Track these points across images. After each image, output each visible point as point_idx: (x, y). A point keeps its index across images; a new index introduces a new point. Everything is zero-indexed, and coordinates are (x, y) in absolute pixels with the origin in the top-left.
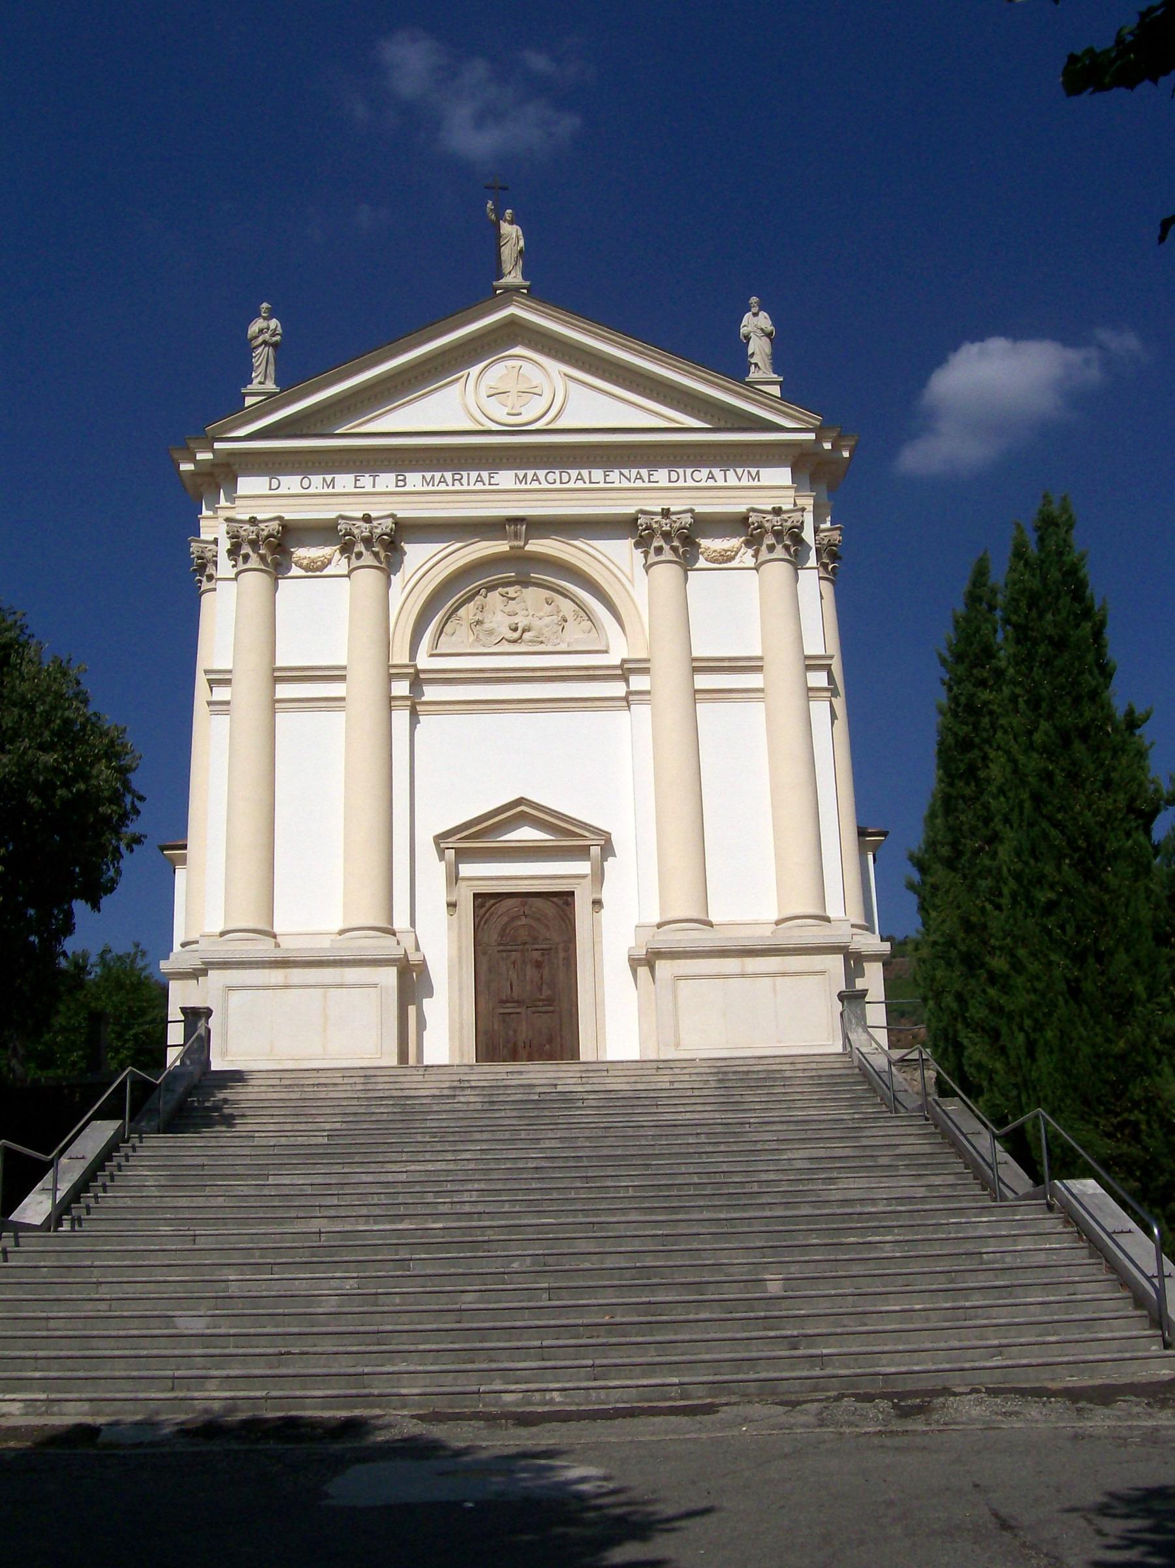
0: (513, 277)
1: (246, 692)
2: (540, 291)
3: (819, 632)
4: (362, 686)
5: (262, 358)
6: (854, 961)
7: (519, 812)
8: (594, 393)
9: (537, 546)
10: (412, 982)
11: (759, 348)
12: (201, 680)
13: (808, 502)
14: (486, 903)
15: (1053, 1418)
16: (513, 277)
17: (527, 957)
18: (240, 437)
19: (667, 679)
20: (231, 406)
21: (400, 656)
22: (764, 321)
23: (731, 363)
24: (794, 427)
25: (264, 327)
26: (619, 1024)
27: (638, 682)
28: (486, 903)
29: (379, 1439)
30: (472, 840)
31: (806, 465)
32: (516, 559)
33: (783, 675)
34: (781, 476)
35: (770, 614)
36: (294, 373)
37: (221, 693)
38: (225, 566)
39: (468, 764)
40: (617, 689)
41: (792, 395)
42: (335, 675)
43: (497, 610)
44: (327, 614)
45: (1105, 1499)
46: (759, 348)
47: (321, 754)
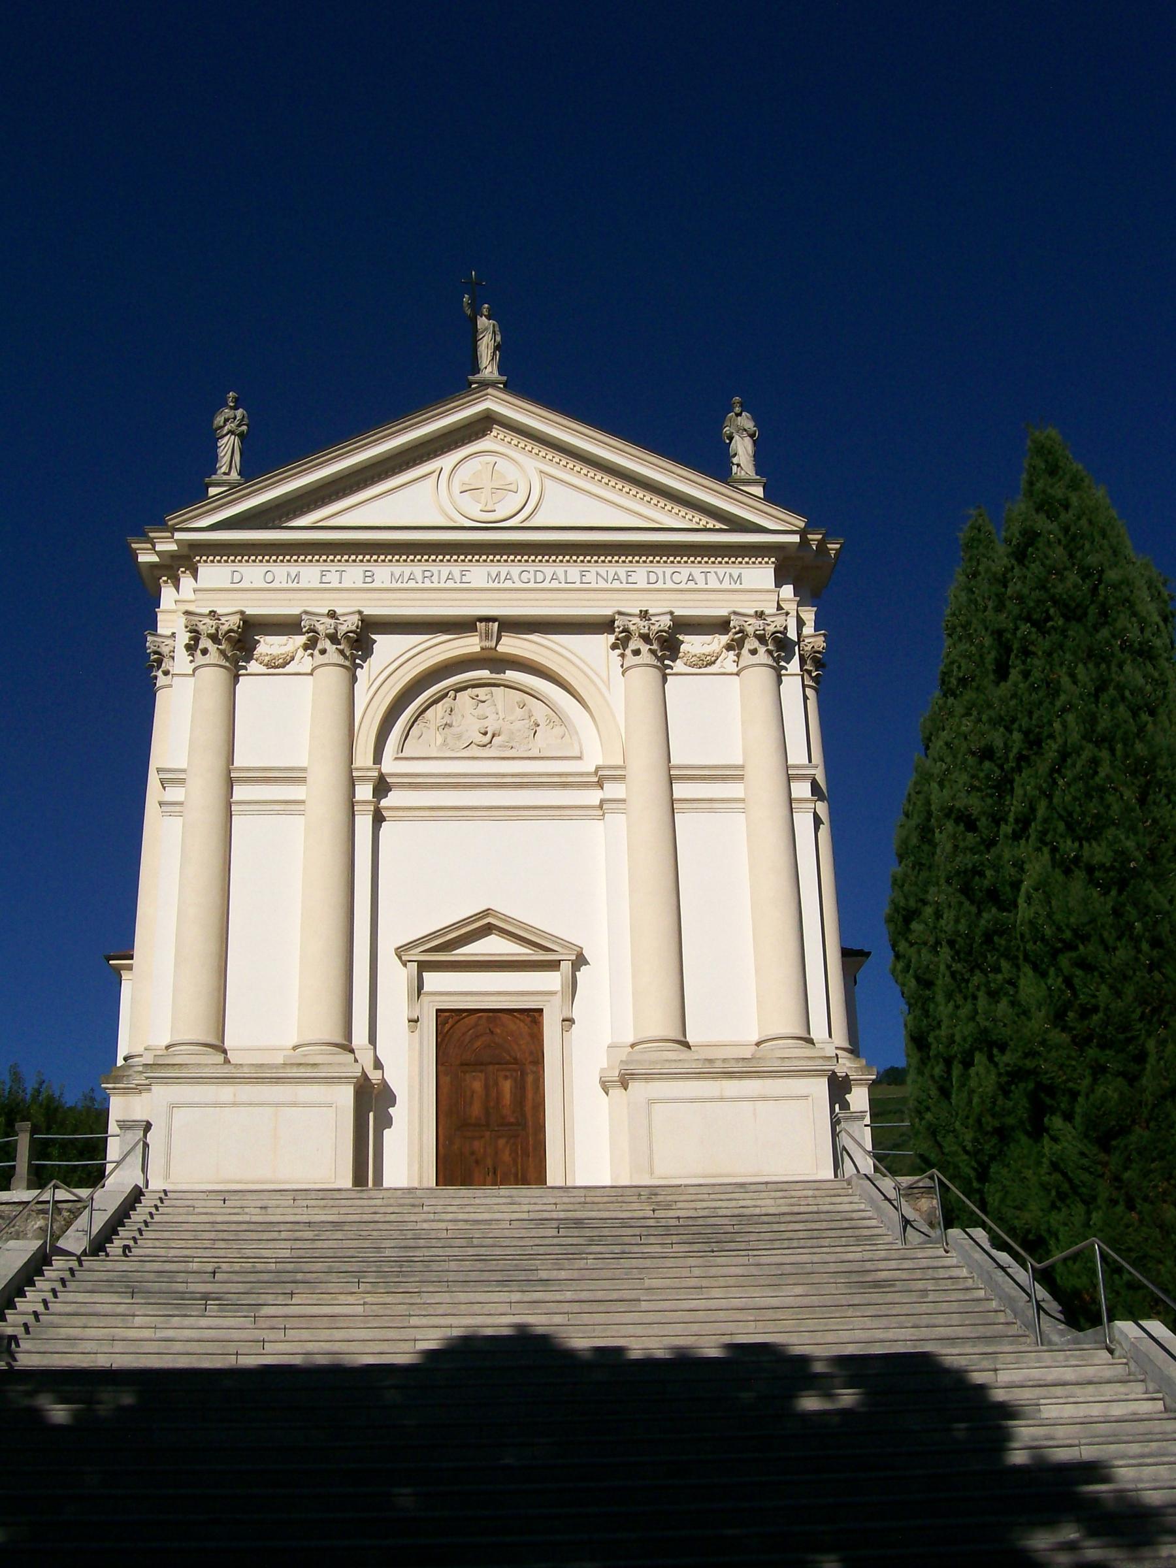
0: (489, 369)
2: (518, 382)
4: (321, 793)
5: (228, 448)
6: (839, 1088)
7: (484, 925)
9: (511, 645)
10: (372, 1101)
11: (743, 450)
12: (153, 780)
13: (809, 615)
14: (451, 1022)
16: (489, 369)
17: (491, 1086)
18: (200, 525)
19: (641, 788)
20: (192, 492)
22: (746, 421)
23: (716, 465)
24: (781, 526)
26: (591, 1140)
27: (613, 790)
28: (451, 1022)
30: (440, 952)
31: (790, 566)
32: (489, 653)
33: (763, 785)
34: (762, 575)
35: (749, 723)
36: (258, 464)
37: (174, 794)
38: (181, 662)
39: (431, 875)
40: (593, 797)
41: (771, 497)
42: (294, 777)
43: (472, 712)
44: (290, 711)
46: (743, 450)
47: (285, 859)
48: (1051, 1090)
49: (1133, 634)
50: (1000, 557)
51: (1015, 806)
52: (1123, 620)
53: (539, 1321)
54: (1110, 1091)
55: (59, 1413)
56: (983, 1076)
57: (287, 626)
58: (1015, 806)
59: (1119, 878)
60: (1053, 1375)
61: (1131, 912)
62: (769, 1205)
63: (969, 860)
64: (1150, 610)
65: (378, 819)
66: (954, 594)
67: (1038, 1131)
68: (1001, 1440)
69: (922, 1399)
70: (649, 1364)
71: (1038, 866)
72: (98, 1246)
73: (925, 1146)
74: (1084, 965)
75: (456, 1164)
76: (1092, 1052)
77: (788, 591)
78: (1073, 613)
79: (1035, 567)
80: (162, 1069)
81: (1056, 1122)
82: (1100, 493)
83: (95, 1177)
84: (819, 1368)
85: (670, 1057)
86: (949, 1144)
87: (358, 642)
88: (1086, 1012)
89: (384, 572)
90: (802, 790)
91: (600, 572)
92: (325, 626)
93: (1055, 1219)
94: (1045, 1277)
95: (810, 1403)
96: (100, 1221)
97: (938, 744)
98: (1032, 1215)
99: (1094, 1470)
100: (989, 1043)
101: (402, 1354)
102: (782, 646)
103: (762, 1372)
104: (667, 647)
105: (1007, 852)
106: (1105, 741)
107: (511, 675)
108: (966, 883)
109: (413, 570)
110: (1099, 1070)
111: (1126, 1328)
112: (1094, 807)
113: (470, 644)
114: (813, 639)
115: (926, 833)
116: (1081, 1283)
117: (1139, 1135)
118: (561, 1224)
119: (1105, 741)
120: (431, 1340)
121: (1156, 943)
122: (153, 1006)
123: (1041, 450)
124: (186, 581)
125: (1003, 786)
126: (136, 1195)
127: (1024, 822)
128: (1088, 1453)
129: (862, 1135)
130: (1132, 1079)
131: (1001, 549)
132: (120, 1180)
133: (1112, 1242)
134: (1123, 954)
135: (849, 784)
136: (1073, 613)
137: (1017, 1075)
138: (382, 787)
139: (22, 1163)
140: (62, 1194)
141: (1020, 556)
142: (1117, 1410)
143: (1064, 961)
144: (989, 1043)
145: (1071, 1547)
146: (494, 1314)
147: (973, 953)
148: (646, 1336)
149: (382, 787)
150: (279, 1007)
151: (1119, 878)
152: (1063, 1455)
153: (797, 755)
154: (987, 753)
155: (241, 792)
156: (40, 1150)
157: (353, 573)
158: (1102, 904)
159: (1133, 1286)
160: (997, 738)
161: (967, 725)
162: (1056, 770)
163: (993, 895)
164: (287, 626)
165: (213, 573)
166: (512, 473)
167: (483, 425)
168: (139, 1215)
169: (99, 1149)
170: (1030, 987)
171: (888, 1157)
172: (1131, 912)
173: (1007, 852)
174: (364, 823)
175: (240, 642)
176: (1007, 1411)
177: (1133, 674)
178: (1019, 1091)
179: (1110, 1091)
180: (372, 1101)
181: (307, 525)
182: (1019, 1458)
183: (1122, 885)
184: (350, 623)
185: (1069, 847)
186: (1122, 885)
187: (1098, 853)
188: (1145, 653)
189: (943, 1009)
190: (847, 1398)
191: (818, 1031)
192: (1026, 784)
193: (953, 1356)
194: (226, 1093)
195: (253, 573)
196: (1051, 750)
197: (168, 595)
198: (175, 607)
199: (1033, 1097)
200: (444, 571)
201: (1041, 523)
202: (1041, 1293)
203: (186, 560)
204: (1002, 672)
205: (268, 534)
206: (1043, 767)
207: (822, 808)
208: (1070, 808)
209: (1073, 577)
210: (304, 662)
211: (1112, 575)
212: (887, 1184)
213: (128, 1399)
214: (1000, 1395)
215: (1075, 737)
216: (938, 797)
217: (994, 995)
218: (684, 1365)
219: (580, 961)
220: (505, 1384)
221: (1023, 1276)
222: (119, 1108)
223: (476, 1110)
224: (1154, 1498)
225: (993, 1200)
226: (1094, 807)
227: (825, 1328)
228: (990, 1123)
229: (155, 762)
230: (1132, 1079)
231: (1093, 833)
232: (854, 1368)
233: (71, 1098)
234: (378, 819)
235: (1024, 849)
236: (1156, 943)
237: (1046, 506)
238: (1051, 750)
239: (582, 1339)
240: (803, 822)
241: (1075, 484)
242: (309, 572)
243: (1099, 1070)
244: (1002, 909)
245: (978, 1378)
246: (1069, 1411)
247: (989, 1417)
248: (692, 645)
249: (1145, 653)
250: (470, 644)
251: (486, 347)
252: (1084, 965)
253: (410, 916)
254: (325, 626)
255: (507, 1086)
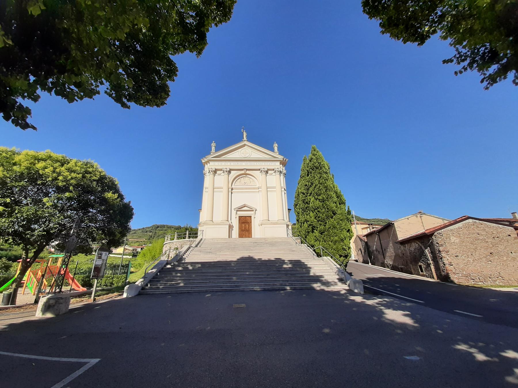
0: (245, 138)
1: (210, 190)
2: (249, 140)
3: (283, 184)
4: (225, 190)
5: (213, 148)
7: (245, 206)
10: (231, 227)
11: (276, 149)
13: (284, 168)
15: (19, 215)
16: (245, 138)
17: (245, 225)
18: (210, 157)
19: (264, 189)
20: (208, 153)
21: (230, 186)
22: (276, 145)
23: (272, 150)
24: (281, 157)
25: (213, 145)
27: (260, 189)
30: (239, 209)
31: (283, 163)
32: (245, 173)
33: (278, 189)
34: (278, 163)
35: (277, 182)
36: (217, 149)
37: (207, 190)
38: (208, 174)
40: (258, 190)
41: (280, 154)
42: (221, 188)
43: (243, 180)
44: (221, 180)
45: (132, 104)
46: (276, 149)
47: (221, 198)
48: (314, 227)
49: (325, 170)
50: (308, 161)
52: (323, 169)
53: (251, 255)
54: (322, 227)
56: (306, 225)
57: (221, 170)
58: (310, 192)
59: (323, 201)
60: (316, 263)
61: (325, 205)
62: (279, 240)
65: (232, 193)
66: (302, 166)
67: (313, 232)
68: (309, 272)
70: (265, 261)
71: (313, 199)
72: (196, 246)
73: (298, 233)
74: (318, 211)
75: (241, 236)
76: (320, 222)
78: (317, 168)
79: (312, 162)
80: (205, 223)
81: (315, 231)
82: (320, 153)
83: (196, 237)
84: (286, 261)
85: (268, 221)
87: (229, 172)
88: (319, 217)
89: (232, 163)
90: (283, 189)
92: (225, 170)
93: (315, 243)
94: (314, 250)
95: (285, 266)
96: (197, 243)
97: (300, 184)
98: (312, 242)
100: (307, 221)
103: (279, 262)
104: (267, 172)
106: (321, 184)
108: (303, 201)
109: (236, 163)
110: (321, 225)
111: (325, 257)
112: (320, 192)
113: (243, 172)
114: (285, 172)
115: (298, 195)
116: (319, 251)
119: (321, 184)
121: (328, 209)
122: (204, 216)
123: (313, 148)
125: (308, 189)
126: (202, 239)
128: (321, 274)
129: (290, 232)
130: (325, 226)
132: (199, 238)
133: (323, 247)
134: (323, 210)
135: (288, 189)
136: (317, 168)
137: (310, 225)
138: (232, 189)
140: (192, 239)
141: (310, 161)
142: (324, 268)
143: (316, 211)
144: (307, 221)
145: (319, 287)
146: (246, 254)
147: (305, 210)
148: (265, 257)
149: (232, 189)
150: (220, 215)
151: (323, 201)
153: (282, 185)
154: (306, 185)
155: (215, 190)
156: (190, 234)
157: (228, 163)
158: (321, 204)
159: (326, 252)
160: (307, 183)
162: (315, 187)
163: (307, 203)
164: (221, 170)
165: (211, 163)
166: (247, 151)
167: (244, 145)
169: (197, 234)
170: (312, 214)
172: (325, 205)
174: (230, 193)
175: (215, 171)
176: (310, 268)
177: (325, 175)
178: (310, 227)
179: (322, 227)
180: (231, 227)
181: (223, 158)
182: (311, 274)
183: (323, 202)
184: (229, 169)
185: (316, 197)
186: (323, 202)
187: (320, 198)
188: (326, 173)
189: (301, 217)
190: (290, 266)
191: (285, 219)
192: (311, 189)
193: (303, 261)
194: (213, 226)
195: (216, 163)
196: (314, 185)
197: (206, 166)
198: (207, 168)
199: (312, 228)
200: (240, 163)
201: (313, 157)
202: (314, 252)
204: (308, 175)
205: (218, 158)
207: (286, 192)
210: (223, 174)
211: (322, 163)
212: (294, 238)
213: (200, 266)
214: (309, 266)
216: (300, 191)
217: (307, 215)
218: (269, 261)
219: (256, 210)
220: (248, 263)
222: (200, 228)
223: (243, 228)
224: (330, 280)
225: (307, 241)
226: (320, 192)
227: (287, 256)
229: (205, 186)
230: (325, 226)
231: (320, 195)
232: (291, 262)
233: (194, 227)
234: (232, 193)
235: (311, 197)
236: (328, 209)
237: (314, 155)
238: (314, 185)
239: (257, 257)
240: (283, 193)
241: (317, 152)
242: (223, 163)
243: (321, 225)
244: (76, 75)
245: (306, 263)
247: (307, 269)
248: (270, 172)
249: (326, 173)
250: (243, 172)
251: (245, 134)
252: (318, 211)
253: (236, 204)
254: (225, 170)
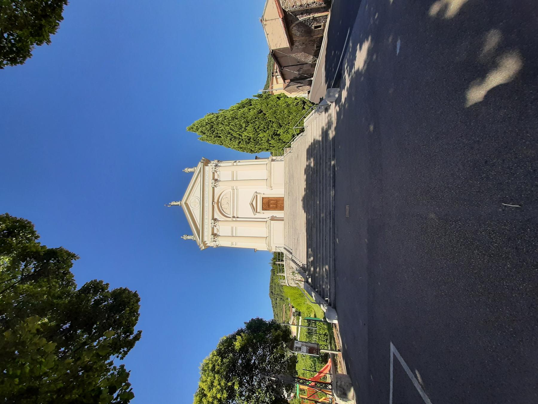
0: (178, 203)
1: (234, 240)
2: (180, 199)
3: (230, 163)
4: (234, 224)
5: (189, 237)
6: (273, 160)
8: (250, 223)
9: (216, 200)
10: (273, 219)
11: (190, 170)
12: (232, 246)
13: (212, 162)
14: (263, 209)
16: (178, 203)
17: (272, 204)
18: (199, 241)
19: (234, 184)
20: (195, 241)
22: (186, 169)
23: (192, 173)
24: (200, 165)
26: (278, 192)
28: (263, 209)
29: (250, 207)
30: (255, 210)
31: (206, 163)
32: (217, 203)
33: (234, 169)
34: (207, 168)
35: (226, 170)
36: (190, 233)
37: (234, 243)
38: (217, 243)
39: (245, 211)
40: (235, 190)
41: (196, 166)
44: (223, 229)
46: (190, 170)
47: (242, 229)
49: (215, 119)
50: (204, 136)
51: (237, 136)
52: (213, 120)
53: (301, 198)
55: (312, 259)
56: (272, 142)
57: (213, 229)
58: (237, 136)
62: (287, 169)
63: (244, 142)
64: (212, 116)
66: (210, 143)
69: (311, 152)
71: (245, 133)
72: (291, 253)
73: (281, 150)
76: (269, 127)
77: (209, 165)
78: (212, 127)
80: (269, 245)
81: (278, 132)
82: (195, 122)
85: (268, 180)
86: (280, 147)
87: (215, 220)
88: (264, 128)
89: (206, 217)
90: (235, 164)
91: (206, 189)
92: (213, 224)
94: (298, 134)
95: (312, 165)
96: (288, 253)
98: (290, 136)
99: (323, 129)
100: (268, 141)
101: (305, 215)
102: (216, 166)
104: (216, 180)
105: (244, 137)
106: (229, 123)
107: (220, 200)
111: (305, 125)
112: (238, 126)
113: (216, 206)
114: (216, 161)
115: (241, 148)
117: (280, 122)
118: (289, 195)
119: (229, 123)
120: (302, 212)
122: (261, 246)
123: (190, 129)
124: (206, 242)
125: (235, 138)
126: (285, 248)
127: (240, 135)
129: (279, 158)
131: (203, 136)
134: (257, 123)
136: (212, 127)
138: (234, 217)
139: (281, 263)
141: (204, 133)
142: (315, 125)
143: (258, 131)
144: (268, 141)
145: (332, 132)
146: (300, 204)
148: (303, 185)
149: (234, 217)
152: (321, 133)
153: (231, 164)
154: (231, 139)
155: (234, 235)
157: (206, 221)
158: (251, 125)
159: (300, 123)
160: (229, 138)
161: (227, 142)
163: (249, 140)
164: (213, 229)
165: (206, 239)
166: (193, 201)
167: (186, 204)
168: (287, 248)
171: (281, 155)
173: (244, 137)
174: (238, 219)
175: (215, 235)
177: (220, 119)
179: (275, 125)
180: (273, 219)
182: (320, 139)
184: (213, 221)
185: (243, 129)
187: (244, 125)
188: (217, 117)
189: (264, 147)
190: (312, 160)
192: (235, 134)
195: (206, 234)
196: (230, 131)
197: (208, 245)
198: (210, 244)
199: (275, 135)
201: (200, 130)
202: (300, 135)
203: (204, 243)
204: (220, 137)
206: (233, 132)
207: (238, 161)
208: (282, 301)
209: (207, 126)
212: (285, 154)
213: (310, 250)
214: (312, 141)
215: (229, 128)
216: (236, 146)
218: (307, 180)
219: (256, 192)
220: (309, 202)
221: (298, 137)
222: (274, 250)
224: (327, 121)
226: (238, 126)
228: (278, 141)
231: (241, 126)
232: (308, 159)
233: (273, 256)
234: (238, 217)
235: (243, 135)
236: (256, 118)
237: (197, 129)
238: (230, 131)
239: (303, 193)
240: (239, 164)
242: (206, 226)
245: (310, 144)
246: (315, 132)
248: (216, 177)
249: (217, 117)
250: (216, 206)
253: (249, 213)
254: (213, 224)
255: (272, 202)
